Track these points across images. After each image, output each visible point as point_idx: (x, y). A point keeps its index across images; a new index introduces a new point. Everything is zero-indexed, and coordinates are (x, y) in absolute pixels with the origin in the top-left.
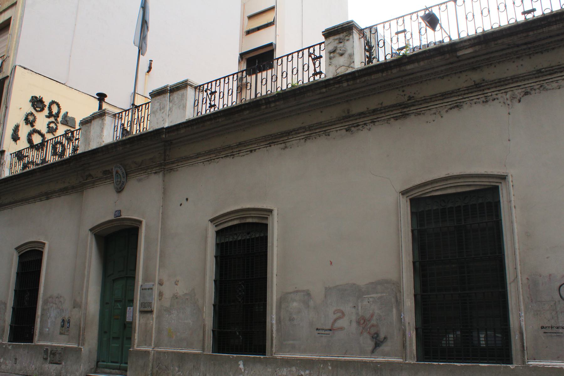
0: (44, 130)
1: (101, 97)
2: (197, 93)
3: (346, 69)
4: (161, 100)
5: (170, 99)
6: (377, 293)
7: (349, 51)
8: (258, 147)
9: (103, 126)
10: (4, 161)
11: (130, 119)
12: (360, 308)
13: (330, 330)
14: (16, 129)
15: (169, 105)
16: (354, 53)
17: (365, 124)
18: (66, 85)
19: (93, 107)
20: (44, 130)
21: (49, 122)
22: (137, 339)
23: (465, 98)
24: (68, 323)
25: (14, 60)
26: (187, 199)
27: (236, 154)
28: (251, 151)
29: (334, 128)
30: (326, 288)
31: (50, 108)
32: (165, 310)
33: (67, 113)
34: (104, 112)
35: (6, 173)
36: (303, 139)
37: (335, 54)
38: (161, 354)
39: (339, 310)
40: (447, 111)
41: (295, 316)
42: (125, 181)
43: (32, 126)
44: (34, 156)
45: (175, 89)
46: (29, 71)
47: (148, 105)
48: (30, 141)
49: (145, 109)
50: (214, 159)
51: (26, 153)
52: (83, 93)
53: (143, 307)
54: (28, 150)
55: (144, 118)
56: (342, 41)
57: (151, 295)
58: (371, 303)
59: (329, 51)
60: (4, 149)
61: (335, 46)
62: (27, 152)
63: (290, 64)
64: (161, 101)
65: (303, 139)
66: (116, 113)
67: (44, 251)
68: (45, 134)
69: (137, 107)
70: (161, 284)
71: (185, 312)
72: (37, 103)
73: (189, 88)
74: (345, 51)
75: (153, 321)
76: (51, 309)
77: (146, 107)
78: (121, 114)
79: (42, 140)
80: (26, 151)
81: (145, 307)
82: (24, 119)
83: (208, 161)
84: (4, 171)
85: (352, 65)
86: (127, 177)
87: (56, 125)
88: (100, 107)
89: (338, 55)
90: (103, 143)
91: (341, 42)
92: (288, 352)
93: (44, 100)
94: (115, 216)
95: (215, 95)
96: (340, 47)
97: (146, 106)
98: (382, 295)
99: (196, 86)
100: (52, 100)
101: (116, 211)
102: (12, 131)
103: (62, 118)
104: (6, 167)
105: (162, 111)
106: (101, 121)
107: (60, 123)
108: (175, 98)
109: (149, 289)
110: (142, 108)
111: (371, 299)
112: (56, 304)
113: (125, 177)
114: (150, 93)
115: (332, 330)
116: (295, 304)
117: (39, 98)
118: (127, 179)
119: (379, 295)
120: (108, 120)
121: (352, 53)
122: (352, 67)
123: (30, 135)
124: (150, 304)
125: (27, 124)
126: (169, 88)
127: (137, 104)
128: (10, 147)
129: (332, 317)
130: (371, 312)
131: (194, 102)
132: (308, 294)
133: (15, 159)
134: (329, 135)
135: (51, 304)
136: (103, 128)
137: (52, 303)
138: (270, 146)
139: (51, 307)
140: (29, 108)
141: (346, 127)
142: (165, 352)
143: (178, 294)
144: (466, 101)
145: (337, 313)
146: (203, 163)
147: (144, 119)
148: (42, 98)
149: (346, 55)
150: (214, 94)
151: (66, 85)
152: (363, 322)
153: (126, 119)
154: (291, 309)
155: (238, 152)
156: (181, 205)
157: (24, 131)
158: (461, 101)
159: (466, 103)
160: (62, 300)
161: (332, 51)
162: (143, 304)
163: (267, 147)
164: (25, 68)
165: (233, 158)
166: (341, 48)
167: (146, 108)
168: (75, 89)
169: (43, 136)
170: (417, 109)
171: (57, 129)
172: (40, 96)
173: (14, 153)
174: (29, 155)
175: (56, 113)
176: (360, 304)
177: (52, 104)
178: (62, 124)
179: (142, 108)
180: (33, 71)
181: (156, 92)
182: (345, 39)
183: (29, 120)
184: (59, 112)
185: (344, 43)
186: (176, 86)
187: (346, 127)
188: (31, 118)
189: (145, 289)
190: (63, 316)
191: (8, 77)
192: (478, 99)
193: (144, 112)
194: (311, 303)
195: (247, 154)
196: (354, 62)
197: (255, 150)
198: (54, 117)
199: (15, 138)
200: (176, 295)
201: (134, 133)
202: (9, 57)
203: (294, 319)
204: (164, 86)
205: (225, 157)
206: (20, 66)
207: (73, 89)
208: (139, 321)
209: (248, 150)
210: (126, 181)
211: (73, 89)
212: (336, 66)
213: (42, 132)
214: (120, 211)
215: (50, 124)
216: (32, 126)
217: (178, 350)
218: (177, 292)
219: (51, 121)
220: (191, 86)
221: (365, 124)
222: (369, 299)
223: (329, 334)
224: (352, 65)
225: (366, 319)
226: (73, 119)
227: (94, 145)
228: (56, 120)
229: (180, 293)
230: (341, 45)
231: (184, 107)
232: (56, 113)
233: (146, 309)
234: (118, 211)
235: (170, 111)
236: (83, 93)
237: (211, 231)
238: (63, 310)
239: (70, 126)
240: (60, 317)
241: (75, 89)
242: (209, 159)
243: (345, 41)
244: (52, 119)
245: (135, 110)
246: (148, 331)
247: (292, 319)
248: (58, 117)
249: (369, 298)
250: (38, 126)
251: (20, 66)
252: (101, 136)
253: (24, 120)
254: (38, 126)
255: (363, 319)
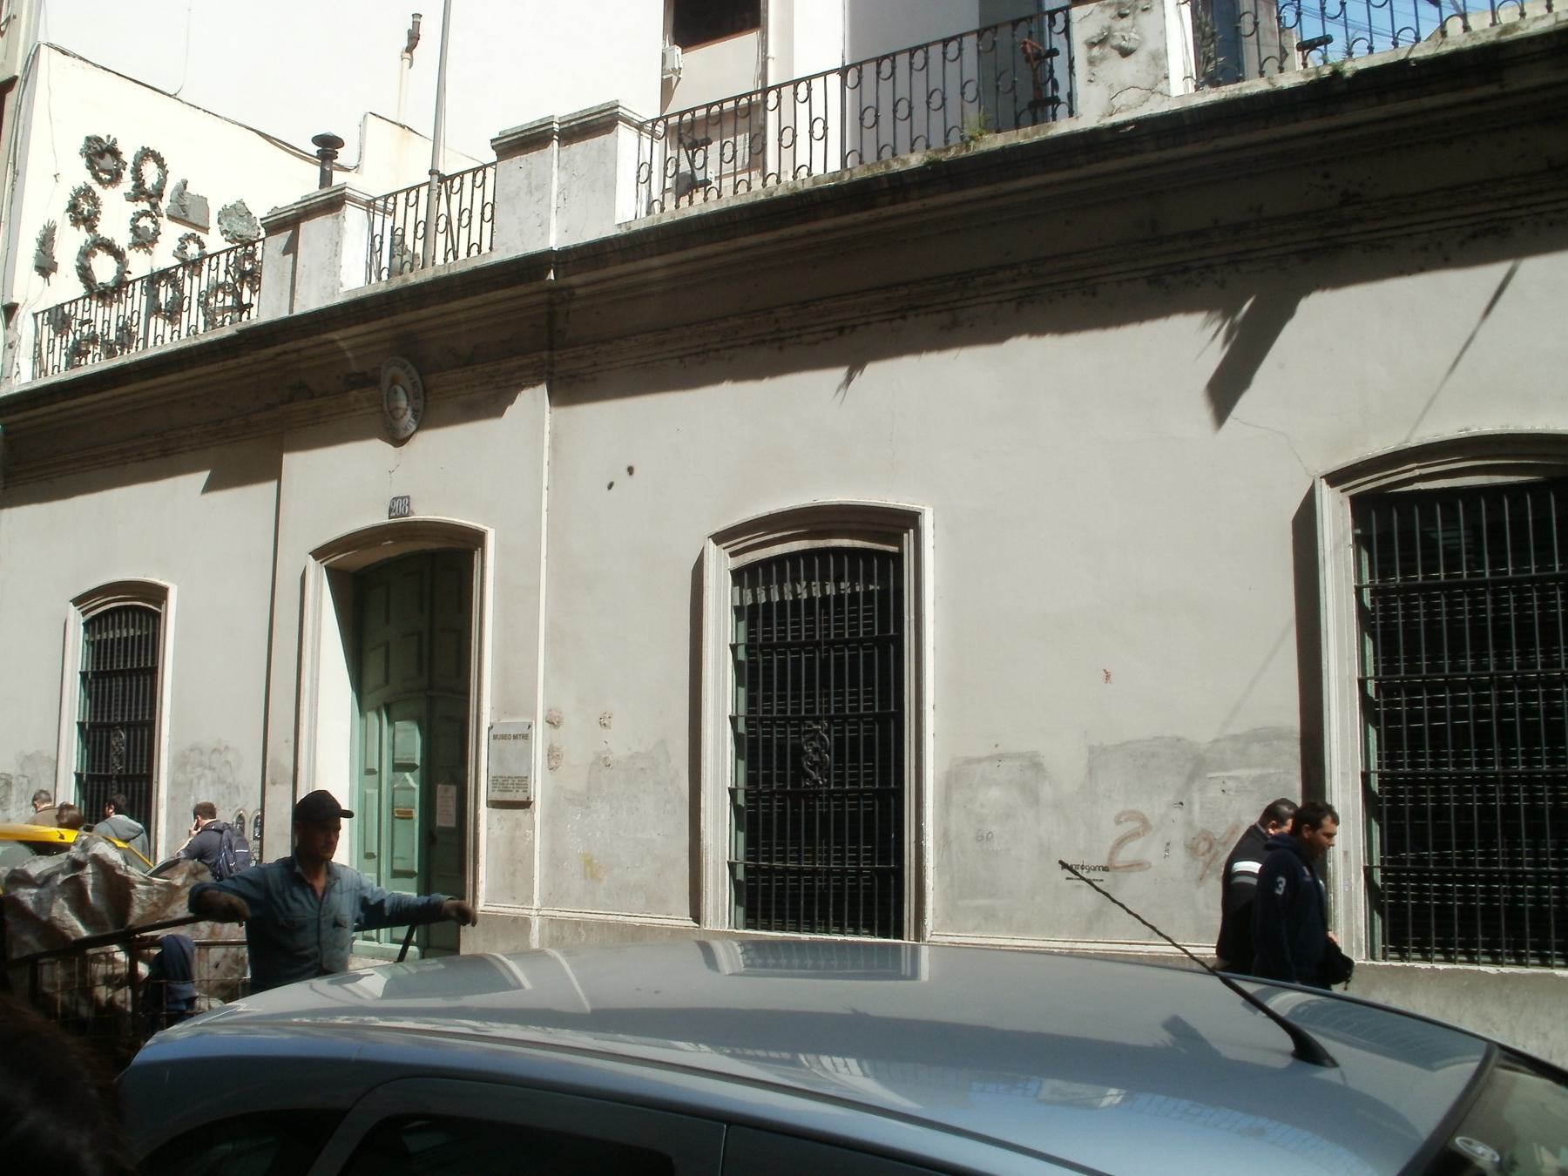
0: (123, 239)
1: (328, 146)
2: (646, 142)
3: (1142, 99)
4: (531, 164)
5: (561, 162)
6: (1249, 766)
7: (1151, 45)
8: (863, 320)
9: (340, 237)
10: (16, 336)
11: (422, 216)
12: (1196, 807)
13: (1106, 869)
14: (47, 240)
15: (558, 178)
16: (1166, 51)
17: (1208, 267)
18: (178, 99)
19: (302, 182)
20: (123, 239)
21: (134, 214)
22: (484, 881)
23: (1519, 208)
24: (256, 826)
25: (34, 28)
26: (631, 470)
27: (791, 337)
28: (841, 331)
29: (1109, 275)
30: (1092, 750)
31: (137, 172)
32: (570, 800)
33: (185, 184)
34: (340, 193)
35: (24, 378)
36: (1010, 300)
37: (1107, 49)
38: (566, 927)
39: (1134, 812)
40: (1462, 243)
41: (995, 829)
42: (421, 408)
43: (91, 228)
44: (105, 319)
45: (576, 129)
46: (76, 61)
47: (481, 173)
48: (85, 274)
49: (473, 186)
50: (717, 350)
51: (83, 310)
52: (226, 119)
53: (499, 791)
54: (90, 304)
55: (471, 212)
56: (1128, 11)
57: (526, 755)
58: (1232, 793)
59: (1085, 39)
60: (15, 300)
61: (1106, 25)
62: (87, 308)
63: (952, 68)
64: (529, 166)
65: (1010, 300)
66: (376, 196)
67: (162, 611)
68: (126, 249)
69: (443, 179)
70: (552, 723)
71: (637, 809)
72: (100, 154)
73: (621, 126)
74: (1141, 42)
75: (534, 832)
76: (199, 783)
77: (474, 181)
78: (391, 200)
79: (118, 268)
80: (84, 305)
81: (506, 790)
82: (67, 206)
83: (697, 354)
84: (18, 367)
85: (1160, 87)
86: (425, 396)
87: (155, 223)
88: (325, 179)
89: (1115, 53)
90: (341, 289)
91: (1123, 16)
92: (975, 929)
93: (120, 147)
94: (393, 514)
95: (706, 152)
96: (1123, 30)
97: (474, 176)
98: (1266, 771)
99: (642, 120)
100: (143, 147)
101: (396, 499)
102: (35, 246)
103: (171, 201)
104: (22, 352)
105: (537, 195)
106: (331, 220)
107: (165, 215)
108: (578, 157)
109: (515, 737)
110: (462, 184)
111: (1231, 784)
112: (212, 769)
113: (422, 397)
114: (492, 141)
115: (1110, 869)
116: (994, 793)
117: (105, 140)
118: (425, 401)
119: (1255, 772)
120: (353, 217)
121: (1162, 50)
122: (1161, 93)
123: (86, 254)
124: (523, 782)
125: (76, 222)
126: (556, 126)
127: (447, 171)
128: (34, 294)
129: (1112, 833)
130: (1231, 820)
131: (636, 170)
132: (1034, 764)
133: (47, 332)
134: (1094, 294)
135: (199, 770)
136: (337, 243)
137: (201, 765)
138: (904, 318)
139: (199, 778)
140: (80, 175)
141: (1148, 273)
142: (577, 923)
143: (611, 753)
144: (1520, 217)
145: (1126, 820)
146: (681, 361)
147: (470, 217)
148: (115, 141)
149: (1141, 56)
150: (704, 148)
151: (178, 99)
152: (1206, 847)
153: (408, 218)
154: (982, 806)
155: (796, 333)
156: (611, 486)
157: (70, 241)
158: (1508, 214)
159: (1522, 224)
160: (230, 757)
161: (1095, 40)
162: (500, 780)
163: (894, 319)
164: (64, 53)
165: (781, 348)
166: (1124, 34)
167: (478, 184)
168: (205, 111)
169: (118, 255)
170: (1369, 232)
171: (157, 233)
172: (109, 136)
173: (44, 312)
174: (93, 318)
175: (155, 184)
176: (1196, 797)
177: (142, 159)
178: (172, 218)
179: (462, 184)
180: (87, 61)
181: (516, 137)
182: (1136, 8)
183: (83, 212)
184: (162, 183)
185: (1135, 18)
186: (580, 121)
187: (1148, 273)
188: (86, 207)
189: (504, 737)
190: (239, 807)
191: (15, 78)
192: (1560, 211)
193: (469, 197)
194: (1046, 792)
195: (827, 339)
196: (1167, 78)
197: (854, 327)
198: (150, 196)
199: (46, 267)
200: (604, 756)
201: (439, 260)
202: (15, 17)
203: (992, 837)
204: (541, 120)
205: (752, 344)
206: (50, 45)
207: (199, 108)
208: (489, 829)
209: (831, 326)
210: (425, 407)
211: (199, 108)
212: (1111, 87)
213: (117, 244)
214: (408, 497)
215: (138, 220)
216: (91, 228)
217: (620, 918)
218: (609, 749)
219: (140, 210)
220: (628, 121)
221: (1208, 267)
222: (1224, 782)
223: (1102, 880)
224: (1160, 87)
225: (1215, 839)
226: (203, 201)
227: (311, 300)
228: (154, 206)
229: (619, 752)
230: (1125, 22)
231: (610, 186)
232: (155, 184)
233: (508, 797)
234: (402, 498)
235: (562, 196)
236: (226, 119)
237: (718, 567)
238: (237, 788)
239: (195, 222)
240: (227, 808)
241: (205, 111)
242: (700, 349)
243: (1139, 11)
244: (145, 206)
245: (440, 187)
246: (520, 861)
247: (983, 837)
248: (160, 196)
249: (1226, 781)
250: (105, 229)
251: (50, 45)
252: (333, 263)
253: (68, 211)
254: (105, 229)
255: (1205, 839)
